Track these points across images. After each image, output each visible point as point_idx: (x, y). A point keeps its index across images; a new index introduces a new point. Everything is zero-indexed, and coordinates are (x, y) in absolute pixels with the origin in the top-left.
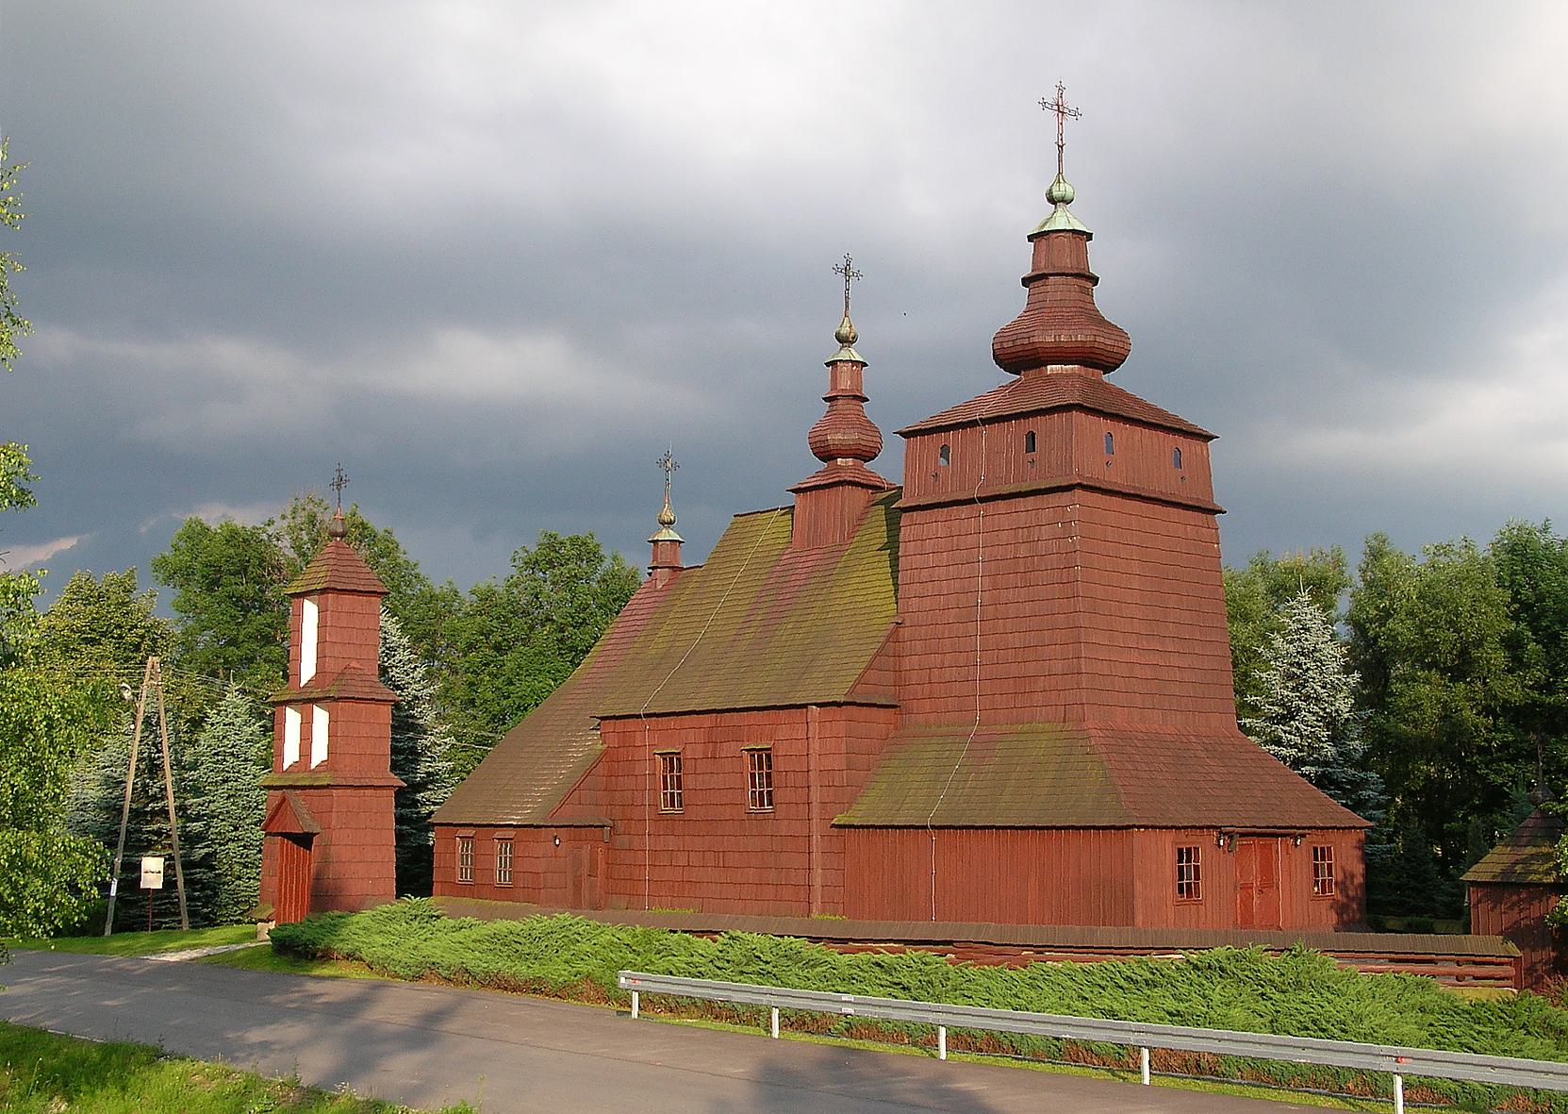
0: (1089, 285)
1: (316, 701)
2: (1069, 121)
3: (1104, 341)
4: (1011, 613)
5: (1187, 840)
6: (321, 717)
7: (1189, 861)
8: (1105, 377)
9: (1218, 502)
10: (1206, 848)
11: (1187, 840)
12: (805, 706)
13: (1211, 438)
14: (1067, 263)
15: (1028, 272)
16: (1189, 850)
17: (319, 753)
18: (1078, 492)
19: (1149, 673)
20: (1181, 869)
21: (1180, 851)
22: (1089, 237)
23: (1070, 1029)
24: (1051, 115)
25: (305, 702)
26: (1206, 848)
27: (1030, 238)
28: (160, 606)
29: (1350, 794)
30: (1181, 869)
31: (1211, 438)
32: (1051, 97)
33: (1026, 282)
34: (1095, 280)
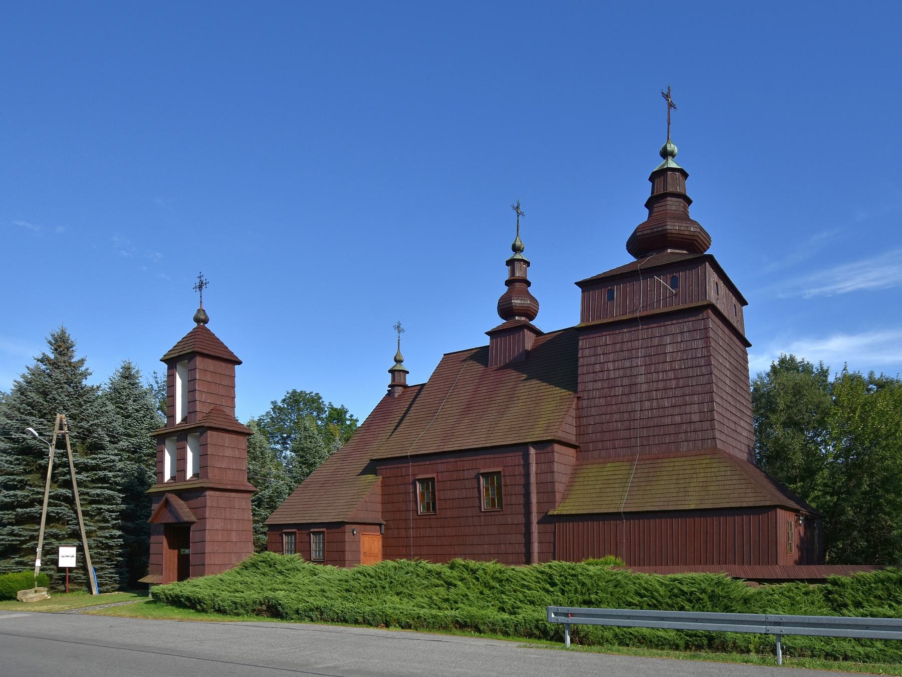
32: (516, 205)
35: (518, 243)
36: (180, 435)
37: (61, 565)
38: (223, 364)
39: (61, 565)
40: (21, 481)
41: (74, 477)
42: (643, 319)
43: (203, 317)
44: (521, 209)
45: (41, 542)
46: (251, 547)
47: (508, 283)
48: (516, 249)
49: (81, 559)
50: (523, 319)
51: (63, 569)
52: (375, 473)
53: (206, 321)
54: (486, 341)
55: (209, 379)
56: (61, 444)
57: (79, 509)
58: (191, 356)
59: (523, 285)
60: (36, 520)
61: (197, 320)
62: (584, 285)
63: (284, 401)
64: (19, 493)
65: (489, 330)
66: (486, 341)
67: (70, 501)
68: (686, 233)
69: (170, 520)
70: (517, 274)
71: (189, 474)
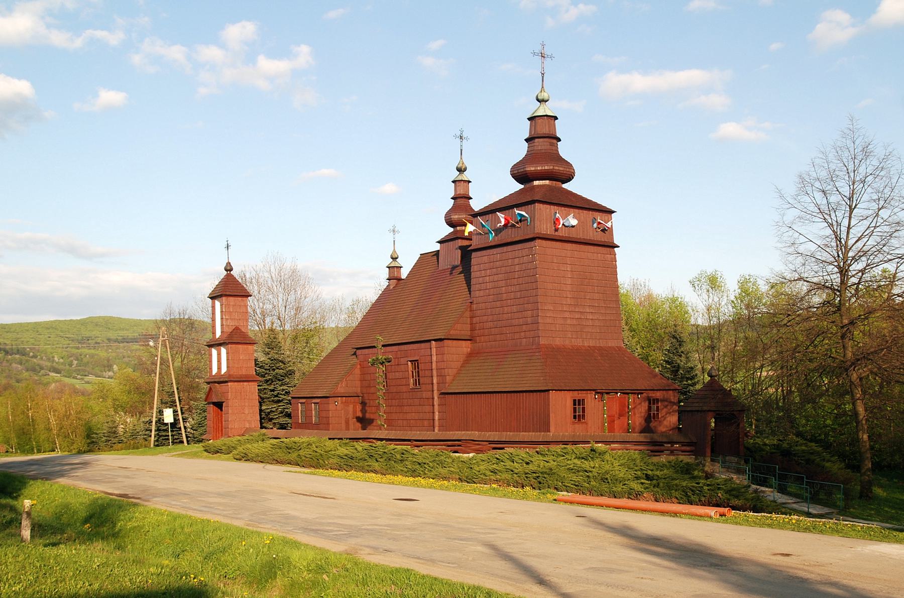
0: (555, 141)
1: (220, 345)
2: (547, 61)
3: (559, 168)
4: (512, 297)
5: (578, 396)
6: (223, 351)
7: (579, 405)
8: (565, 186)
9: (616, 242)
10: (591, 401)
11: (578, 396)
12: (429, 341)
13: (614, 212)
14: (545, 131)
15: (527, 136)
16: (583, 400)
17: (224, 369)
18: (538, 242)
19: (575, 322)
21: (575, 401)
22: (556, 118)
23: (560, 497)
24: (458, 140)
25: (217, 344)
26: (591, 401)
27: (453, 182)
28: (689, 365)
29: (753, 393)
30: (575, 409)
31: (614, 212)
32: (458, 134)
33: (527, 140)
34: (559, 140)
44: (464, 135)
48: (461, 170)
53: (231, 270)
54: (437, 247)
61: (226, 270)
65: (439, 239)
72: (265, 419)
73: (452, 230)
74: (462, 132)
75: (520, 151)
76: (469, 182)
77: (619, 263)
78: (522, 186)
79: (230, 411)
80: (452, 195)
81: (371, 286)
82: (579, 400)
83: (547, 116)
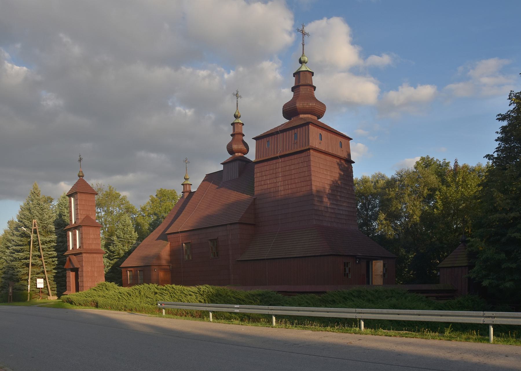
20: (345, 269)
21: (345, 263)
32: (235, 93)
35: (237, 114)
36: (76, 228)
37: (38, 287)
38: (89, 196)
39: (38, 287)
40: (22, 249)
41: (41, 246)
42: (281, 157)
43: (81, 175)
44: (239, 94)
45: (30, 276)
46: (104, 279)
47: (232, 135)
48: (236, 117)
49: (45, 283)
50: (240, 154)
51: (39, 288)
52: (166, 239)
53: (83, 176)
54: (221, 168)
55: (83, 203)
56: (35, 232)
57: (44, 261)
58: (76, 193)
59: (240, 136)
60: (27, 265)
61: (79, 176)
62: (256, 139)
63: (156, 196)
64: (21, 254)
65: (222, 162)
66: (221, 168)
67: (40, 257)
68: (307, 107)
69: (72, 267)
70: (236, 131)
71: (78, 247)
72: (109, 278)
73: (231, 156)
74: (238, 92)
75: (288, 95)
76: (243, 124)
77: (354, 169)
78: (288, 121)
79: (84, 275)
80: (232, 132)
81: (491, 145)
82: (347, 263)
83: (308, 71)
